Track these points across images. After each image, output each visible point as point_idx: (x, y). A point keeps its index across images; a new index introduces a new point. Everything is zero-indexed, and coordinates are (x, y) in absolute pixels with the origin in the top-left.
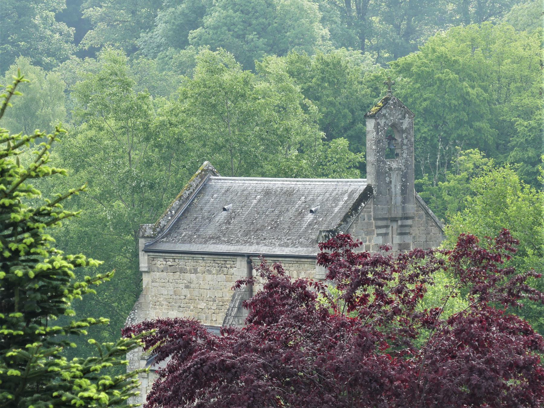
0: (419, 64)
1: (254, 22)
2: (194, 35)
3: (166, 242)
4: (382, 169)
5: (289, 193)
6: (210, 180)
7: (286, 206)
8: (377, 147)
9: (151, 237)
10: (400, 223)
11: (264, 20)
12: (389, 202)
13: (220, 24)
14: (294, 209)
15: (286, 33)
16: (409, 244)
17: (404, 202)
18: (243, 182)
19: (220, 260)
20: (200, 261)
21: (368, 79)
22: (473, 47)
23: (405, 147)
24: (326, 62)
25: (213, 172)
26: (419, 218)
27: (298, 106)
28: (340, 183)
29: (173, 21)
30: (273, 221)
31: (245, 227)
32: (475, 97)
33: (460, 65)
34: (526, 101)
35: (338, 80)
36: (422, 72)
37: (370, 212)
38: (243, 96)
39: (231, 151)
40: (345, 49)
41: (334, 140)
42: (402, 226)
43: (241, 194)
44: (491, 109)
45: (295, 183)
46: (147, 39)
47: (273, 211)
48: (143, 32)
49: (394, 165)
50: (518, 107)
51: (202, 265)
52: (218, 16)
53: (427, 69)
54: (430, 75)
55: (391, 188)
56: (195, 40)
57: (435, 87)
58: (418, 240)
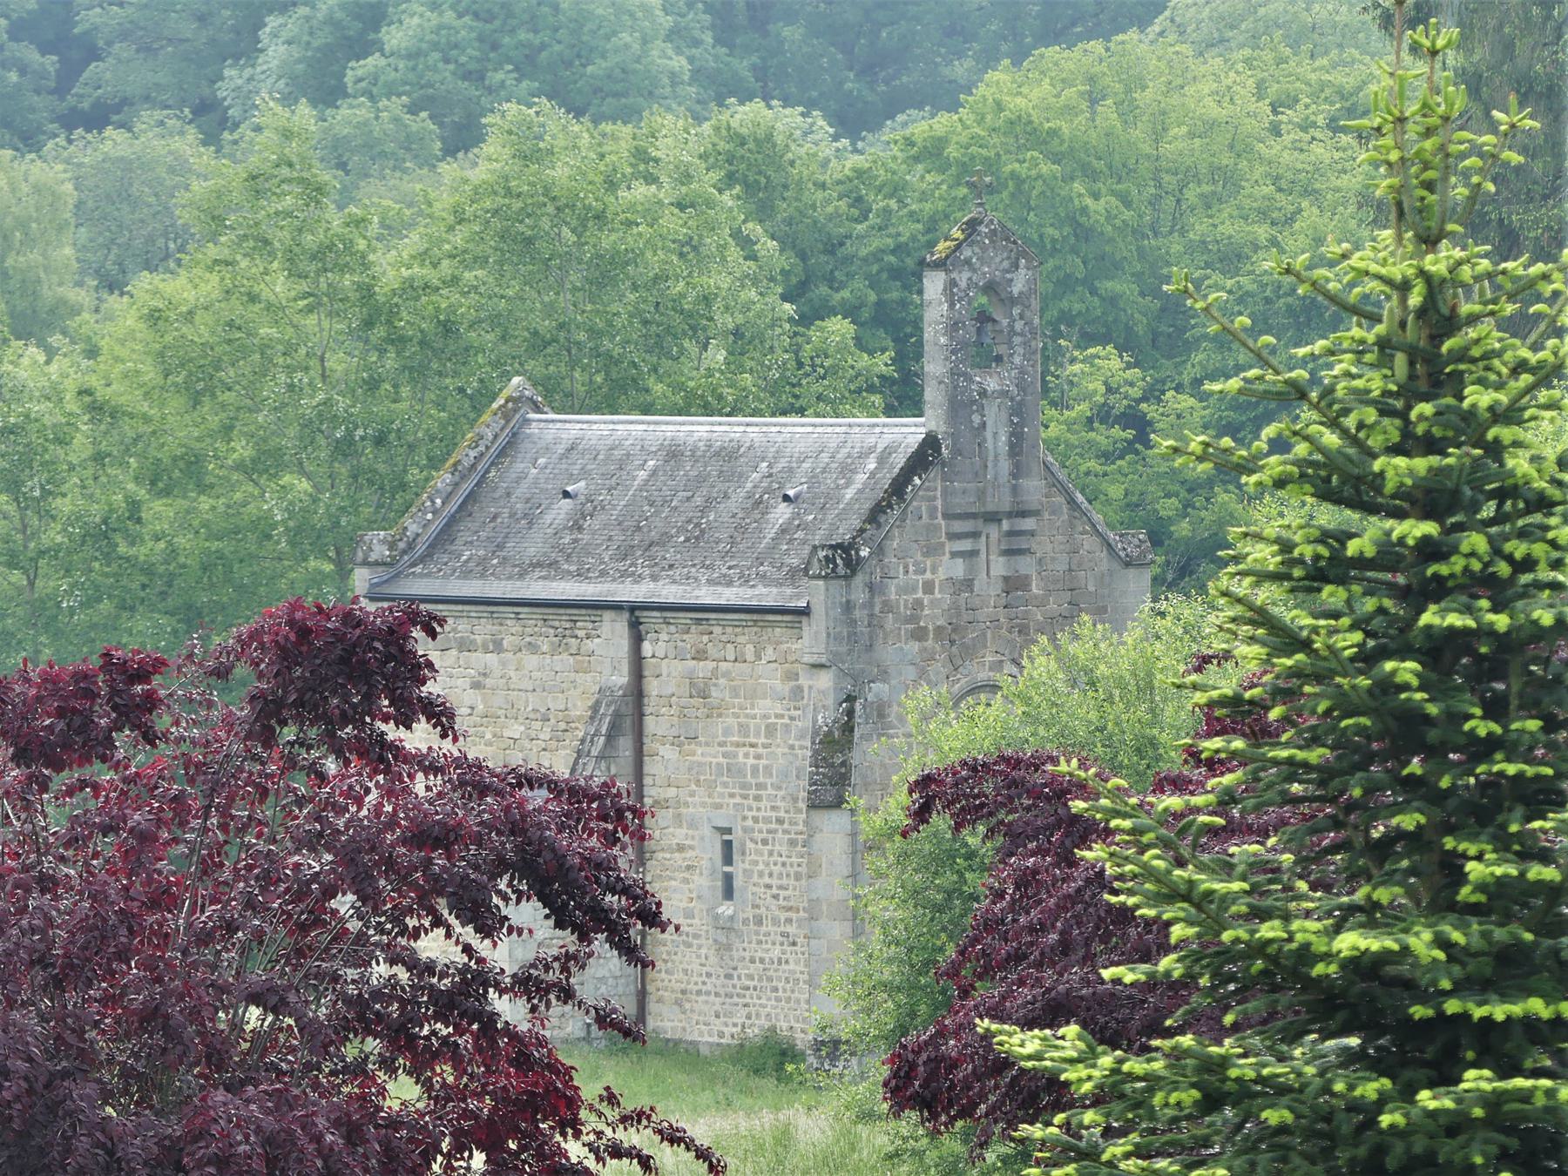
0: (964, 139)
1: (507, 40)
2: (360, 73)
3: (422, 576)
4: (962, 393)
5: (728, 455)
6: (528, 421)
7: (721, 486)
8: (952, 338)
9: (385, 564)
10: (1006, 525)
11: (531, 36)
12: (979, 475)
13: (424, 46)
14: (742, 493)
15: (584, 66)
16: (1027, 577)
17: (1017, 472)
18: (611, 427)
19: (561, 620)
20: (509, 622)
21: (840, 176)
22: (1094, 100)
23: (1017, 340)
24: (737, 134)
25: (535, 403)
26: (1053, 513)
27: (730, 240)
28: (857, 430)
29: (306, 38)
30: (689, 521)
31: (619, 537)
32: (1102, 220)
33: (1063, 141)
34: (1227, 229)
35: (768, 178)
36: (973, 158)
37: (935, 498)
38: (600, 217)
39: (569, 351)
40: (762, 104)
41: (818, 323)
42: (1011, 534)
43: (607, 458)
44: (1140, 250)
45: (742, 429)
46: (240, 82)
47: (688, 499)
48: (230, 66)
49: (992, 384)
50: (1204, 242)
51: (513, 630)
52: (420, 26)
53: (984, 152)
54: (991, 165)
55: (985, 440)
56: (363, 84)
57: (1005, 194)
58: (1050, 567)
